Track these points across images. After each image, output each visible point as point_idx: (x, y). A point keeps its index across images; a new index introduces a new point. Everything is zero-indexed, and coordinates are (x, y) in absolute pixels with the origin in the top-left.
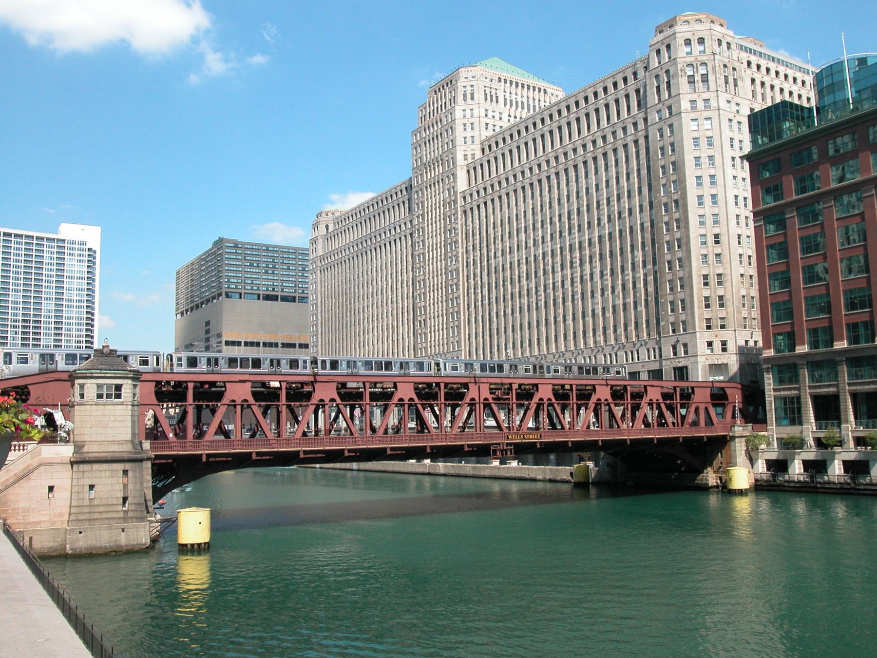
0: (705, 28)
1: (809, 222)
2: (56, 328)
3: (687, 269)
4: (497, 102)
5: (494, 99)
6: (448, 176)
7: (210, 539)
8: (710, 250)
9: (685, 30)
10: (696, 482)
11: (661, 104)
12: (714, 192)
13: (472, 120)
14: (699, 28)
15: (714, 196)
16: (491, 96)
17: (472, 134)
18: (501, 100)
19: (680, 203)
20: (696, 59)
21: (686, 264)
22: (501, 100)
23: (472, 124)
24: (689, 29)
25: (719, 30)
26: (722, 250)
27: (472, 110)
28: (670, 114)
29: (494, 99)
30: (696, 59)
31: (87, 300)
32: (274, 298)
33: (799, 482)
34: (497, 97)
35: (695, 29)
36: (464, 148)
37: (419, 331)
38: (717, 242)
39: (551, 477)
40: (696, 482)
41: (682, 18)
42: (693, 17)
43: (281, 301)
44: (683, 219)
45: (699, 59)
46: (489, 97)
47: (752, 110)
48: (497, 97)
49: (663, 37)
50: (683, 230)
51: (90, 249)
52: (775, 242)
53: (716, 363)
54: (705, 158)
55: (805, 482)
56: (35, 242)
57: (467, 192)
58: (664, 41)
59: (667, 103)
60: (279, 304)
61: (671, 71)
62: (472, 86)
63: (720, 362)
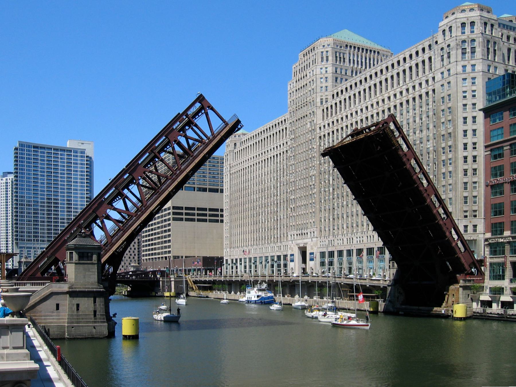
0: (476, 15)
1: (496, 159)
2: (68, 204)
3: (454, 179)
4: (344, 61)
5: (342, 60)
6: (310, 113)
7: (91, 297)
8: (470, 166)
9: (462, 16)
10: (432, 312)
11: (444, 68)
12: (474, 127)
13: (326, 75)
14: (472, 15)
15: (474, 131)
16: (340, 58)
17: (326, 85)
18: (347, 60)
19: (452, 135)
20: (468, 37)
21: (454, 175)
22: (347, 60)
23: (326, 78)
24: (464, 16)
25: (486, 16)
26: (478, 166)
27: (326, 68)
28: (449, 74)
29: (342, 60)
30: (468, 37)
31: (86, 182)
32: (205, 190)
33: (498, 314)
34: (344, 59)
35: (469, 16)
36: (320, 94)
37: (291, 215)
38: (475, 161)
39: (358, 308)
40: (432, 312)
41: (461, 8)
42: (469, 7)
43: (209, 192)
44: (453, 145)
45: (470, 36)
46: (338, 59)
47: (506, 71)
48: (344, 59)
49: (448, 21)
50: (453, 153)
51: (87, 157)
52: (496, 165)
53: (469, 239)
54: (470, 104)
55: (502, 314)
56: (53, 152)
57: (322, 124)
58: (448, 24)
59: (448, 67)
60: (207, 193)
61: (451, 45)
62: (327, 52)
63: (472, 239)
